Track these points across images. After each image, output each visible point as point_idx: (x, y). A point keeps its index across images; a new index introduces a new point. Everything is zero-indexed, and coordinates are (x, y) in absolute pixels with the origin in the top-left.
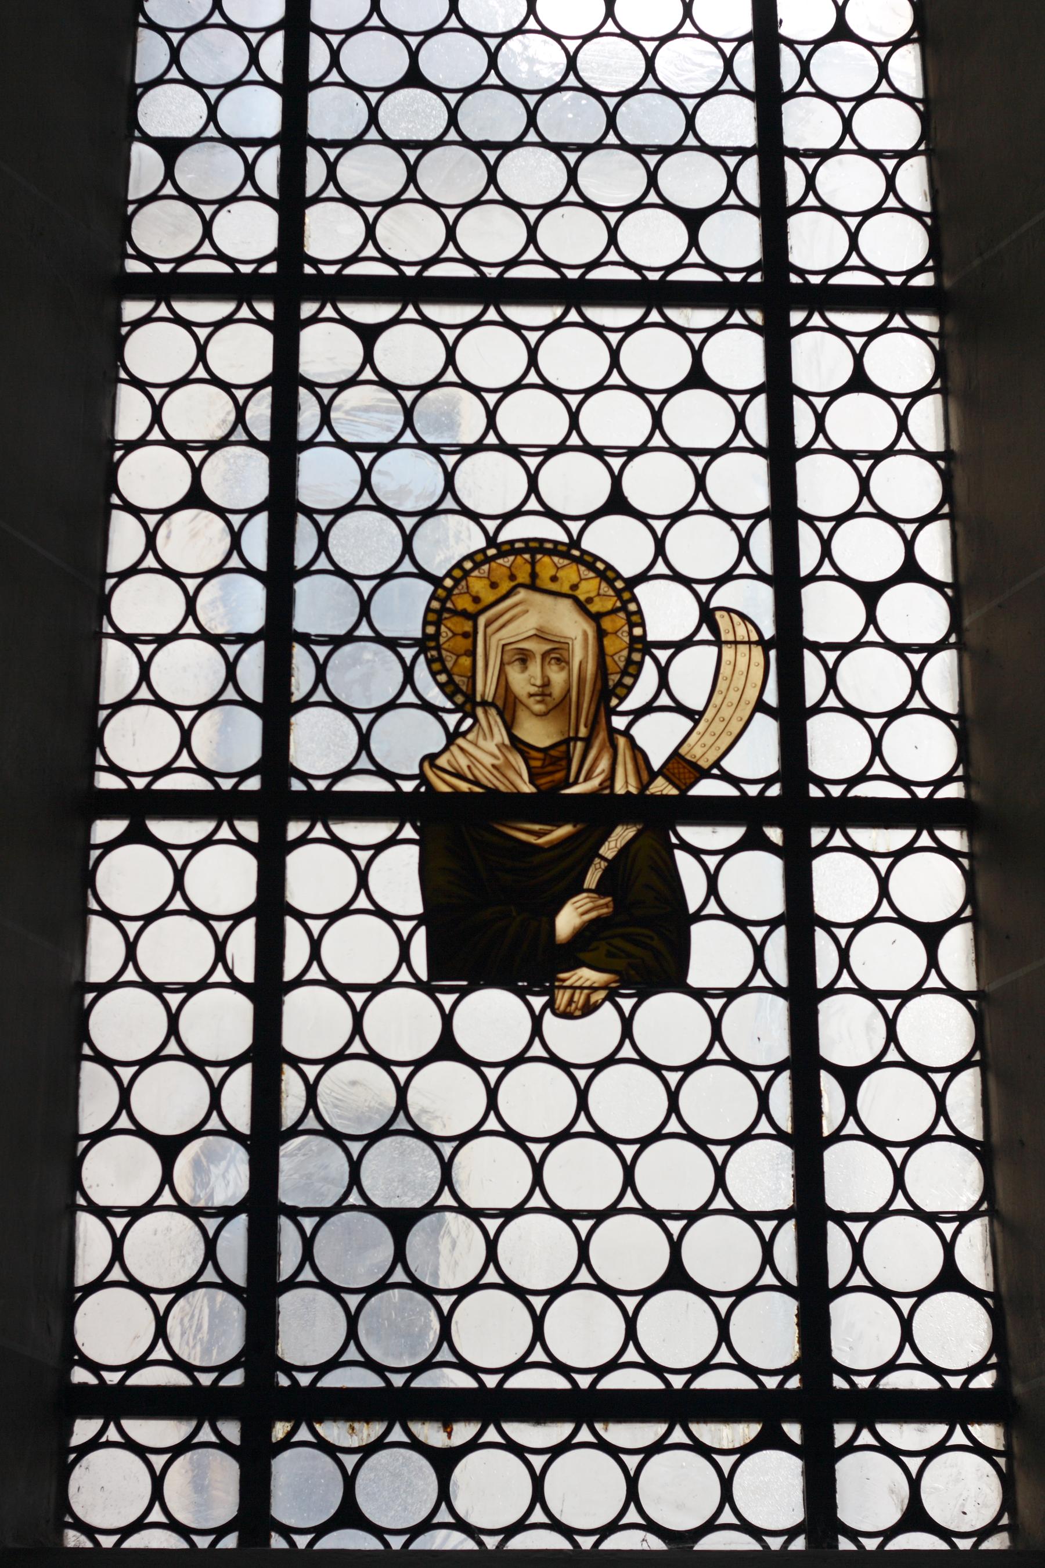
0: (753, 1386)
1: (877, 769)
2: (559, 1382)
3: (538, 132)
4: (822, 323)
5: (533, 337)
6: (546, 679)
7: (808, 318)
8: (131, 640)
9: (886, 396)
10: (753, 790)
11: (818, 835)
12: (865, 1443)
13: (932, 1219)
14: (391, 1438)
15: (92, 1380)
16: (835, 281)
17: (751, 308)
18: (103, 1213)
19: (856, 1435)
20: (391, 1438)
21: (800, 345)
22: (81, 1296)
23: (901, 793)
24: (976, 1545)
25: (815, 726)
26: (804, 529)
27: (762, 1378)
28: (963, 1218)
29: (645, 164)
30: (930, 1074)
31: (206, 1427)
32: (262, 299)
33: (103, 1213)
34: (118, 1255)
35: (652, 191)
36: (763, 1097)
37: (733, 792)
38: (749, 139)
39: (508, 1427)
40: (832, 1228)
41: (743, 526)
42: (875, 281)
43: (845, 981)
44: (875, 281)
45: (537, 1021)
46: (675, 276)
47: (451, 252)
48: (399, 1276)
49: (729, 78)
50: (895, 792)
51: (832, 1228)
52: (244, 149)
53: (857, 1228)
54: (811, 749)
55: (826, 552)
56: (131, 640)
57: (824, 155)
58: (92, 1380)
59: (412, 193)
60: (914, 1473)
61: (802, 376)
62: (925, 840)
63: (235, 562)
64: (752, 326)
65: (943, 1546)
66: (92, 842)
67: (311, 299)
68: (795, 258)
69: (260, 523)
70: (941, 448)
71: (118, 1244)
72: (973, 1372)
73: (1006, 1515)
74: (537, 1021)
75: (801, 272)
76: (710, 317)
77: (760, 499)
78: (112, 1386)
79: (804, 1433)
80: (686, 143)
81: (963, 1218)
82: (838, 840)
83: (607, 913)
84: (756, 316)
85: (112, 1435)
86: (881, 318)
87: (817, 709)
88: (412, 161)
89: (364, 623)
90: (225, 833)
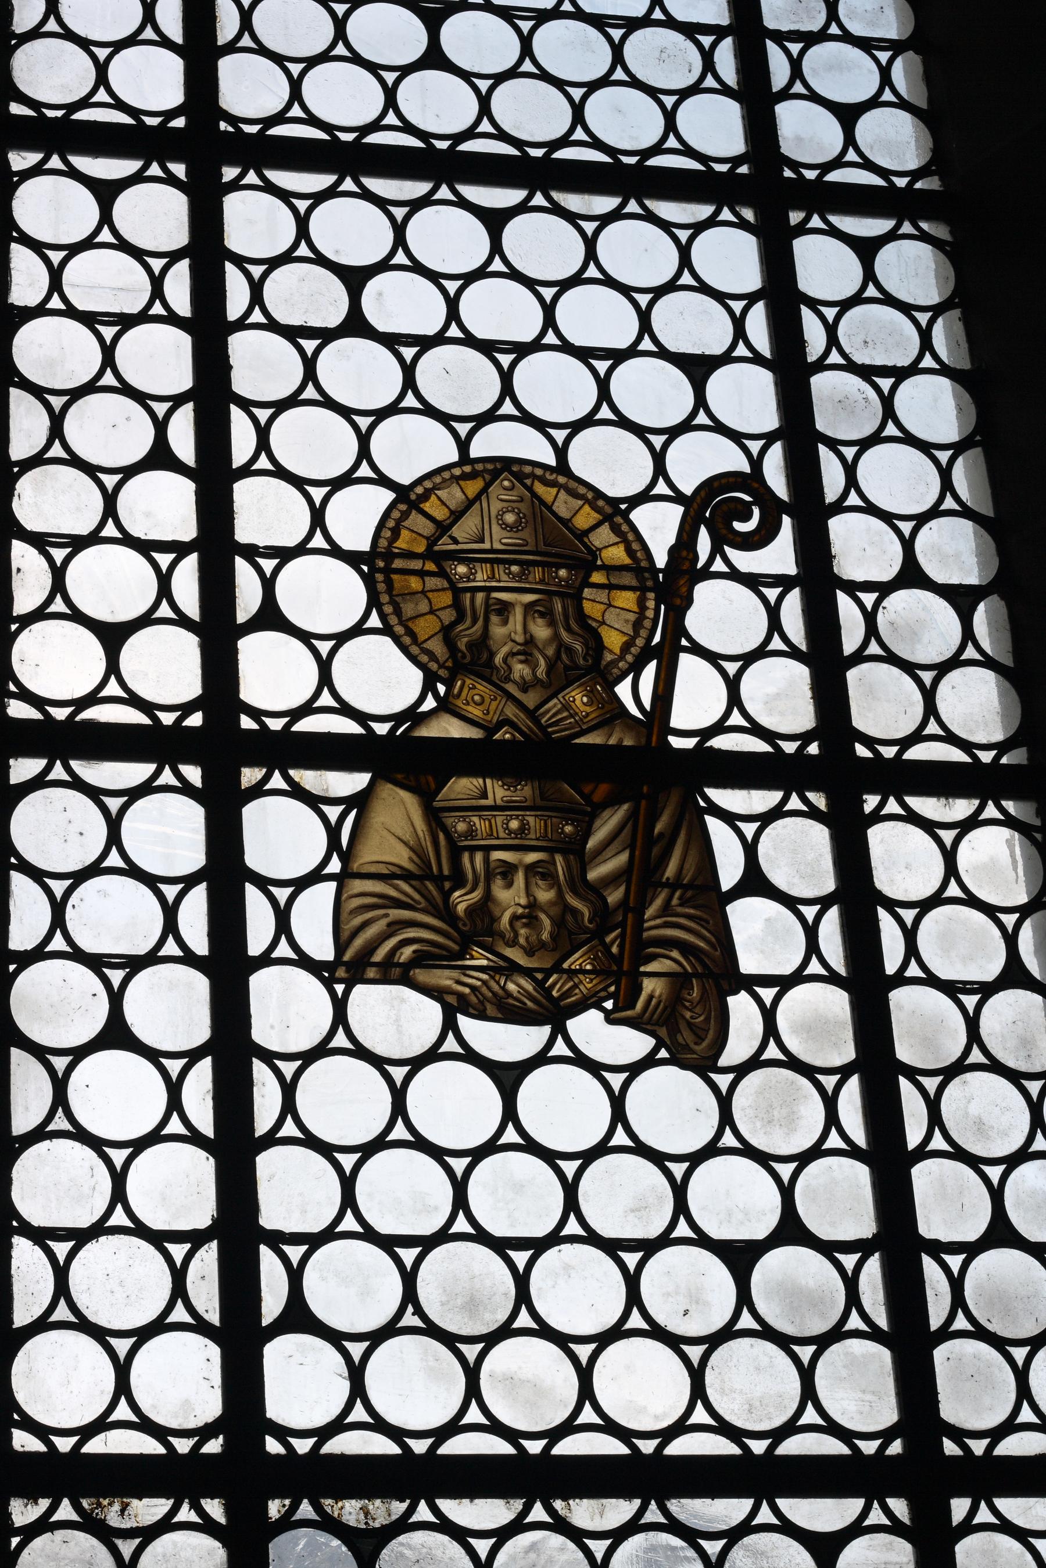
0: (161, 1450)
2: (152, 1446)
6: (528, 635)
14: (533, 203)
15: (39, 1447)
18: (41, 1236)
19: (973, 1511)
20: (533, 203)
31: (423, 1506)
32: (816, 789)
34: (62, 1289)
36: (289, 1107)
39: (445, 1505)
40: (266, 1253)
42: (877, 181)
44: (877, 181)
47: (326, 699)
51: (266, 1253)
58: (39, 1447)
59: (57, 451)
64: (813, 813)
69: (198, 897)
70: (365, 546)
71: (61, 1273)
78: (65, 1454)
79: (228, 1511)
82: (984, 1515)
83: (431, 884)
85: (765, 1516)
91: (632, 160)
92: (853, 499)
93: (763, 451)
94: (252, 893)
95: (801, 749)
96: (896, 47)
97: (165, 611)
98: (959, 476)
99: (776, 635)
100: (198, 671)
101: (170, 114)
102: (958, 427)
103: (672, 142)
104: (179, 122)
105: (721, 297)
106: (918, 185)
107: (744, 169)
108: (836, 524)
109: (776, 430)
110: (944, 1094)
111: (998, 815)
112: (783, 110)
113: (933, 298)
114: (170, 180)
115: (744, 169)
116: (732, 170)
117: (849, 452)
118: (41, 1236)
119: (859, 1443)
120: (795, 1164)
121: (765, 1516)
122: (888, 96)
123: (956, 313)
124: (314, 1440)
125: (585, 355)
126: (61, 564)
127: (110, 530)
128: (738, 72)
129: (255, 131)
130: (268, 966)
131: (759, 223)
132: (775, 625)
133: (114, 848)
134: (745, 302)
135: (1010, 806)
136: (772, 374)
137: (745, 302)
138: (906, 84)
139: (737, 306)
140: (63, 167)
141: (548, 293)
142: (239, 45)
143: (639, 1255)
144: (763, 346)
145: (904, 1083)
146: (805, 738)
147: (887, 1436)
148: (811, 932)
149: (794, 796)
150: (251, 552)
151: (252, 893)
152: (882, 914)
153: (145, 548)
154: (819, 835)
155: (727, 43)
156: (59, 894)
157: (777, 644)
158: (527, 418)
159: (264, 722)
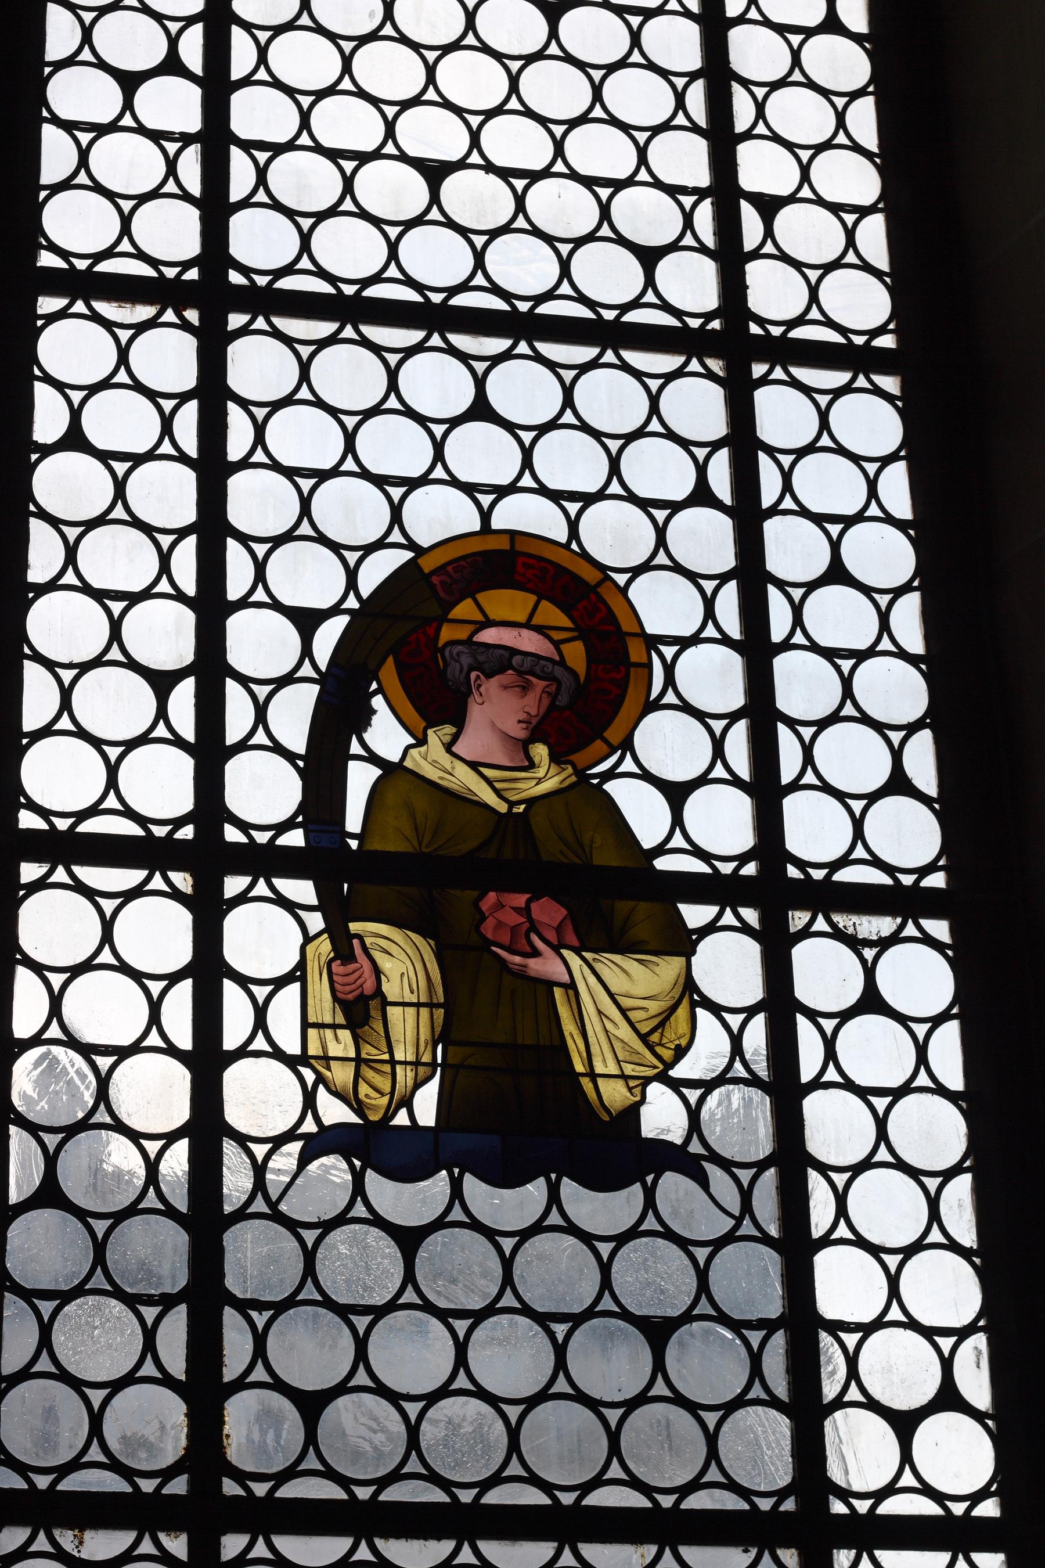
1: (860, 852)
3: (404, 532)
7: (770, 371)
8: (69, 127)
11: (758, 370)
12: (851, 1335)
13: (929, 1333)
14: (343, 335)
20: (343, 335)
21: (802, 954)
23: (884, 879)
24: (918, 881)
25: (791, 804)
26: (815, 1180)
28: (962, 1334)
30: (833, 142)
35: (598, 106)
38: (193, 123)
41: (701, 453)
43: (809, 778)
47: (393, 272)
49: (701, 460)
50: (878, 877)
52: (938, 1340)
53: (851, 1340)
54: (761, 428)
55: (808, 759)
56: (69, 127)
60: (893, 1270)
61: (787, 700)
62: (910, 930)
63: (171, 187)
65: (887, 880)
66: (47, 59)
67: (761, 360)
72: (976, 1498)
73: (944, 858)
76: (668, 362)
77: (717, 426)
80: (657, 561)
81: (962, 1334)
87: (826, 1241)
89: (805, 161)
90: (169, 316)
92: (761, 129)
97: (797, 594)
100: (818, 1285)
101: (178, 823)
105: (664, 73)
110: (128, 1546)
111: (68, 880)
120: (423, 98)
121: (910, 930)
122: (681, 120)
124: (271, 277)
125: (589, 182)
126: (407, 1286)
127: (305, 140)
130: (120, 231)
133: (479, 271)
141: (797, 76)
143: (355, 163)
146: (709, 317)
151: (773, 591)
153: (156, 136)
156: (260, 555)
159: (353, 1492)
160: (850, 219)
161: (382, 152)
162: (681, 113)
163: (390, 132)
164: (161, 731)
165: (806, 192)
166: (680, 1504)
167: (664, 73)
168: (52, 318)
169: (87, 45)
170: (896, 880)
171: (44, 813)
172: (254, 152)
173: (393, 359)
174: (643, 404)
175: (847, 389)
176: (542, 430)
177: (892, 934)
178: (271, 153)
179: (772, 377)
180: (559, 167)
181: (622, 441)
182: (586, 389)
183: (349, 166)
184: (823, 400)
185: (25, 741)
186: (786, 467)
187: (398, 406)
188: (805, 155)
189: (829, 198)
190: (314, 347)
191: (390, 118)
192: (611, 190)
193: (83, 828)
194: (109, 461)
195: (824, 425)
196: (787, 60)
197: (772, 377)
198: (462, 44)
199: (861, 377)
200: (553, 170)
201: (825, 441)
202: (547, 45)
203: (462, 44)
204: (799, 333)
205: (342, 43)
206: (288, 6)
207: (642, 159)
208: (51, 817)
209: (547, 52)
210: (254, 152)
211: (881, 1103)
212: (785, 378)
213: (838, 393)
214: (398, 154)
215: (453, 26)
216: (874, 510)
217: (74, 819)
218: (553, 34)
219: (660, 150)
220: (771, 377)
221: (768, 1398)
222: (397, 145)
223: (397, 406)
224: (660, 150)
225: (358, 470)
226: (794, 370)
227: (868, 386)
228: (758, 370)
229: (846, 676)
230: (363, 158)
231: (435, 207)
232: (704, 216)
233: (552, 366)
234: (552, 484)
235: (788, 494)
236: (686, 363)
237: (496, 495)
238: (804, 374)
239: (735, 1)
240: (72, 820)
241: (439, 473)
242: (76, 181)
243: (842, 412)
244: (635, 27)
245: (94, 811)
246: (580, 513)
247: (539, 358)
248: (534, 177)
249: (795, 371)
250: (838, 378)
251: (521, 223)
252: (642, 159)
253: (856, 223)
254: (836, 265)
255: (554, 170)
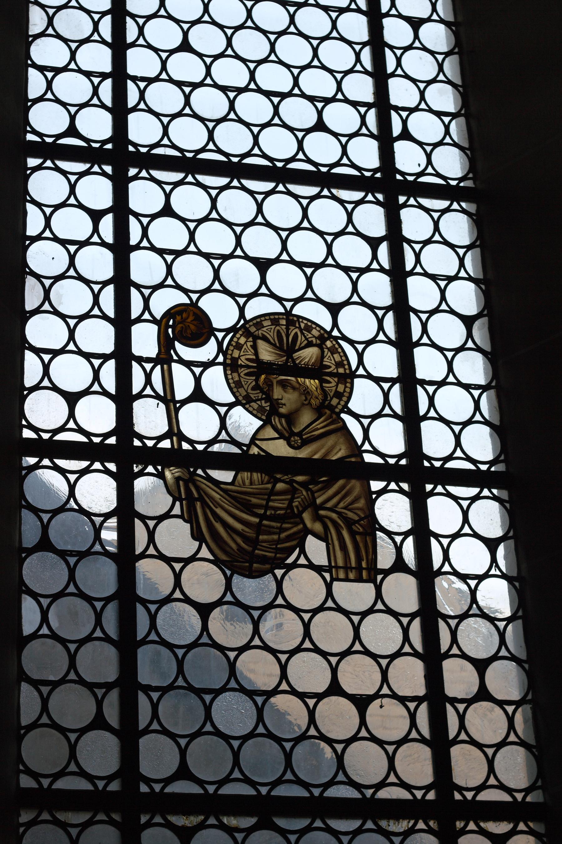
4: (458, 208)
5: (214, 193)
8: (42, 69)
9: (81, 206)
10: (392, 461)
16: (200, 156)
17: (463, 201)
18: (38, 351)
22: (30, 173)
27: (397, 489)
29: (46, 77)
32: (379, 192)
33: (36, 684)
37: (472, 467)
38: (107, 68)
45: (329, 587)
46: (155, 151)
47: (301, 156)
48: (490, 752)
57: (150, 81)
58: (34, 785)
64: (378, 203)
67: (134, 166)
68: (132, 136)
69: (110, 290)
74: (329, 587)
75: (135, 145)
84: (380, 197)
86: (272, 185)
88: (49, 78)
91: (97, 145)
93: (409, 623)
94: (133, 291)
95: (397, 462)
96: (454, 116)
98: (453, 127)
99: (380, 317)
101: (106, 436)
102: (532, 713)
103: (345, 161)
104: (109, 146)
105: (350, 43)
106: (462, 184)
107: (378, 175)
108: (410, 281)
109: (385, 235)
112: (386, 22)
113: (467, 242)
114: (104, 174)
115: (378, 175)
116: (373, 175)
117: (399, 52)
118: (38, 351)
119: (388, 459)
123: (478, 250)
125: (312, 99)
128: (396, 332)
129: (191, 156)
131: (398, 341)
132: (363, 122)
134: (409, 618)
135: (464, 205)
136: (415, 580)
137: (409, 618)
138: (473, 268)
139: (357, 48)
140: (53, 166)
142: (145, 19)
144: (398, 409)
145: (412, 315)
146: (375, 171)
147: (400, 457)
148: (380, 322)
149: (370, 195)
150: (135, 79)
151: (133, 291)
152: (405, 245)
153: (88, 74)
154: (379, 212)
155: (397, 387)
156: (47, 286)
157: (381, 337)
158: (272, 295)
160: (320, 105)
161: (160, 78)
162: (141, 38)
163: (73, 57)
164: (96, 387)
165: (164, 76)
166: (52, 786)
167: (350, 43)
168: (36, 169)
169: (165, 284)
170: (91, 440)
171: (36, 430)
172: (442, 117)
173: (260, 197)
174: (254, 208)
175: (181, 183)
176: (200, 222)
177: (474, 502)
178: (146, 83)
179: (140, 176)
180: (164, 76)
181: (421, 245)
182: (315, 209)
183: (276, 100)
184: (350, 207)
185: (25, 393)
186: (417, 251)
187: (308, 226)
188: (208, 60)
189: (435, 108)
190: (91, 103)
191: (296, 75)
192: (280, 98)
193: (57, 438)
194: (66, 245)
195: (437, 228)
196: (244, 14)
197: (140, 176)
198: (69, 5)
199: (370, 195)
200: (205, 82)
201: (305, 224)
202: (159, 10)
203: (69, 5)
204: (293, 165)
205: (312, 41)
206: (152, 6)
207: (422, 98)
208: (40, 433)
209: (159, 14)
210: (442, 117)
211: (178, 566)
212: (148, 176)
213: (312, 199)
214: (343, 98)
215: (197, 12)
216: (239, 252)
217: (156, 441)
218: (416, 36)
219: (432, 92)
220: (277, 190)
221: (161, 729)
222: (212, 79)
223: (308, 226)
224: (432, 92)
225: (52, 236)
226: (420, 200)
227: (284, 190)
228: (402, 199)
229: (220, 341)
230: (195, 86)
231: (142, 102)
232: (371, 117)
233: (427, 210)
234: (61, 236)
235: (375, 261)
236: (366, 196)
237: (78, 246)
238: (158, 174)
239: (385, 5)
240: (155, 441)
241: (47, 234)
242: (139, 107)
243: (315, 209)
244: (292, 13)
245: (62, 429)
246: (173, 261)
247: (153, 179)
248: (283, 96)
249: (244, 182)
250: (313, 191)
251: (276, 121)
252: (422, 98)
253: (146, 87)
254: (264, 126)
255: (206, 82)
